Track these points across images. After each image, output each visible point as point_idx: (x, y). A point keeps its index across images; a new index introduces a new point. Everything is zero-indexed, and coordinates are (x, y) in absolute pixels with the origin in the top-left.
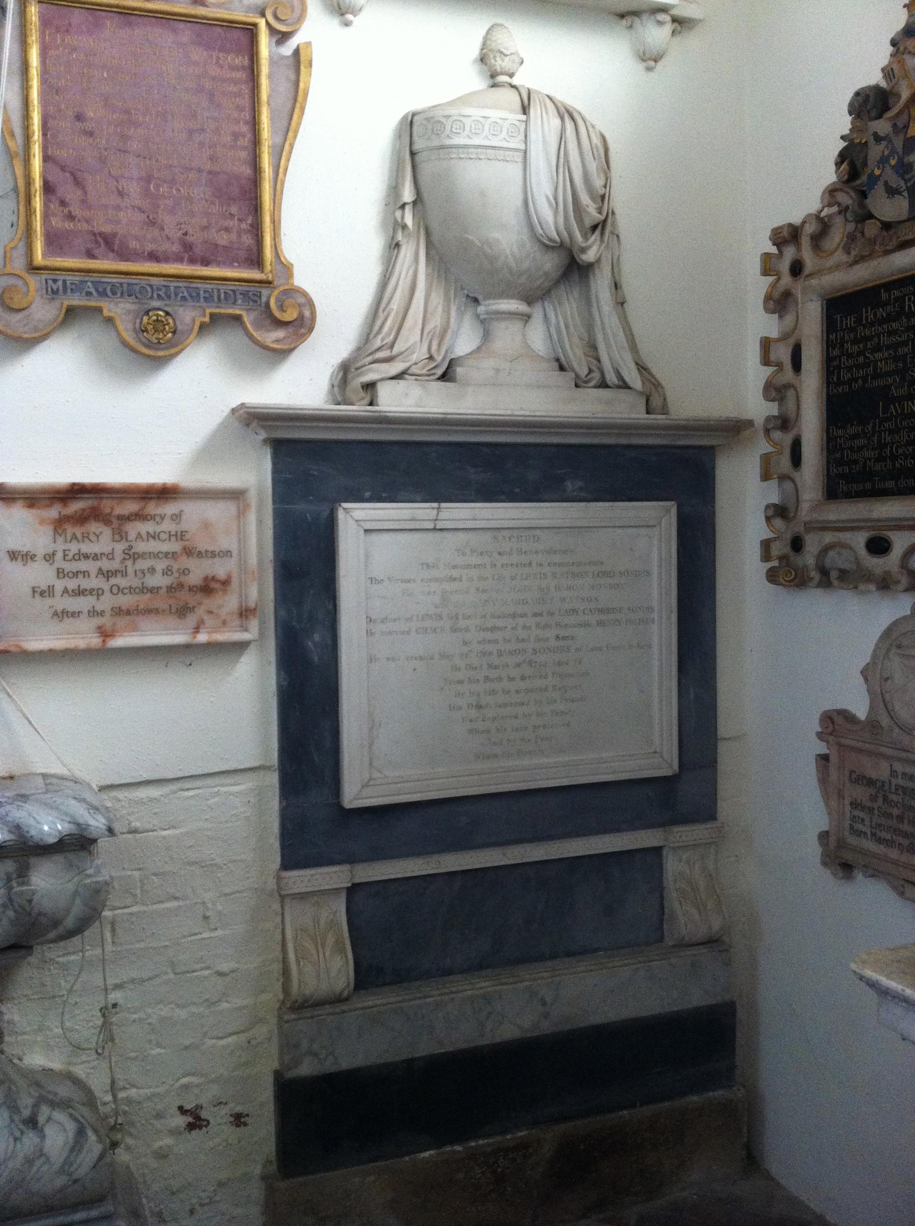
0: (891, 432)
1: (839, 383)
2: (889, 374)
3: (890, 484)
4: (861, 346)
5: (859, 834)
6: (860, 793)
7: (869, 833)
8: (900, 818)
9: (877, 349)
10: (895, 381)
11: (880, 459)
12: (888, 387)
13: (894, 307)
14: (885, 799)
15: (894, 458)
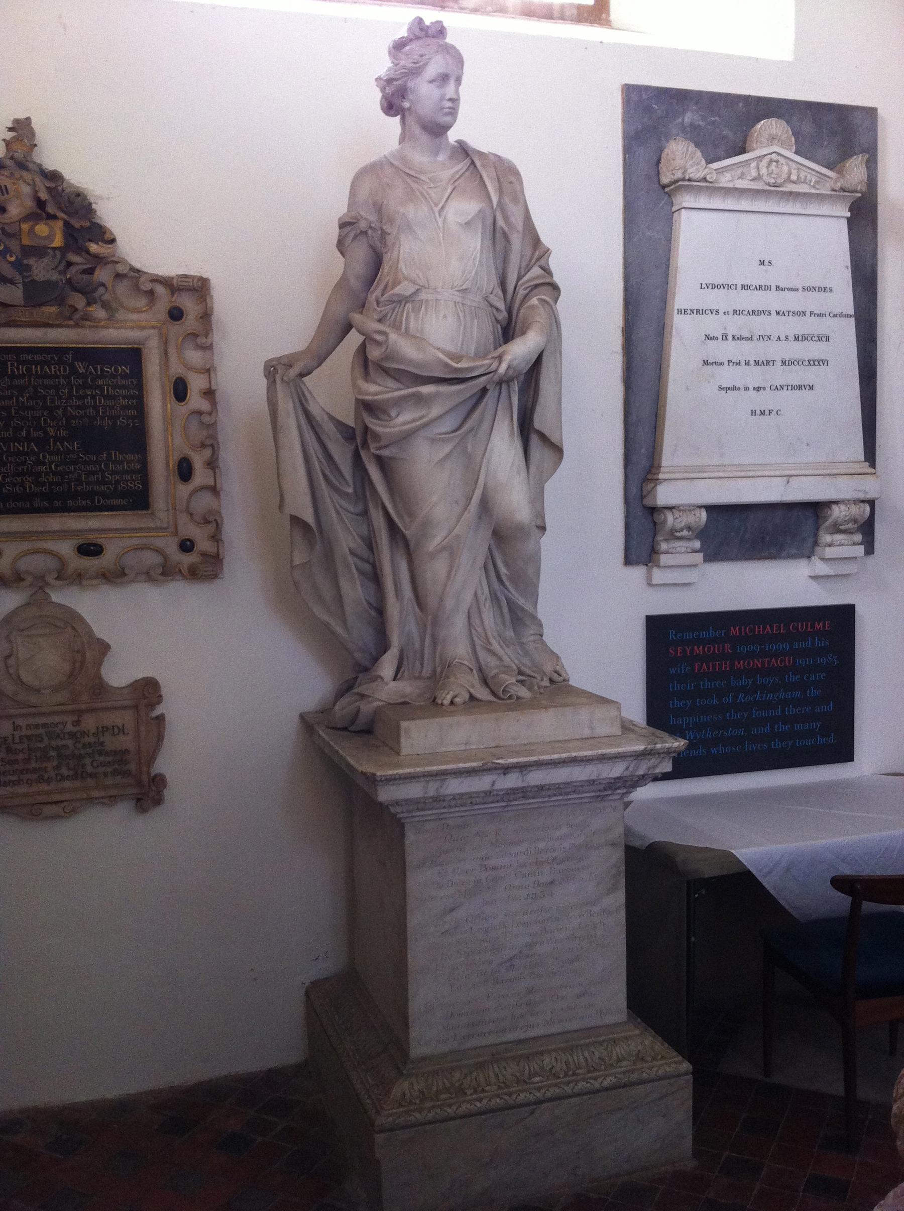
14: (9, 750)
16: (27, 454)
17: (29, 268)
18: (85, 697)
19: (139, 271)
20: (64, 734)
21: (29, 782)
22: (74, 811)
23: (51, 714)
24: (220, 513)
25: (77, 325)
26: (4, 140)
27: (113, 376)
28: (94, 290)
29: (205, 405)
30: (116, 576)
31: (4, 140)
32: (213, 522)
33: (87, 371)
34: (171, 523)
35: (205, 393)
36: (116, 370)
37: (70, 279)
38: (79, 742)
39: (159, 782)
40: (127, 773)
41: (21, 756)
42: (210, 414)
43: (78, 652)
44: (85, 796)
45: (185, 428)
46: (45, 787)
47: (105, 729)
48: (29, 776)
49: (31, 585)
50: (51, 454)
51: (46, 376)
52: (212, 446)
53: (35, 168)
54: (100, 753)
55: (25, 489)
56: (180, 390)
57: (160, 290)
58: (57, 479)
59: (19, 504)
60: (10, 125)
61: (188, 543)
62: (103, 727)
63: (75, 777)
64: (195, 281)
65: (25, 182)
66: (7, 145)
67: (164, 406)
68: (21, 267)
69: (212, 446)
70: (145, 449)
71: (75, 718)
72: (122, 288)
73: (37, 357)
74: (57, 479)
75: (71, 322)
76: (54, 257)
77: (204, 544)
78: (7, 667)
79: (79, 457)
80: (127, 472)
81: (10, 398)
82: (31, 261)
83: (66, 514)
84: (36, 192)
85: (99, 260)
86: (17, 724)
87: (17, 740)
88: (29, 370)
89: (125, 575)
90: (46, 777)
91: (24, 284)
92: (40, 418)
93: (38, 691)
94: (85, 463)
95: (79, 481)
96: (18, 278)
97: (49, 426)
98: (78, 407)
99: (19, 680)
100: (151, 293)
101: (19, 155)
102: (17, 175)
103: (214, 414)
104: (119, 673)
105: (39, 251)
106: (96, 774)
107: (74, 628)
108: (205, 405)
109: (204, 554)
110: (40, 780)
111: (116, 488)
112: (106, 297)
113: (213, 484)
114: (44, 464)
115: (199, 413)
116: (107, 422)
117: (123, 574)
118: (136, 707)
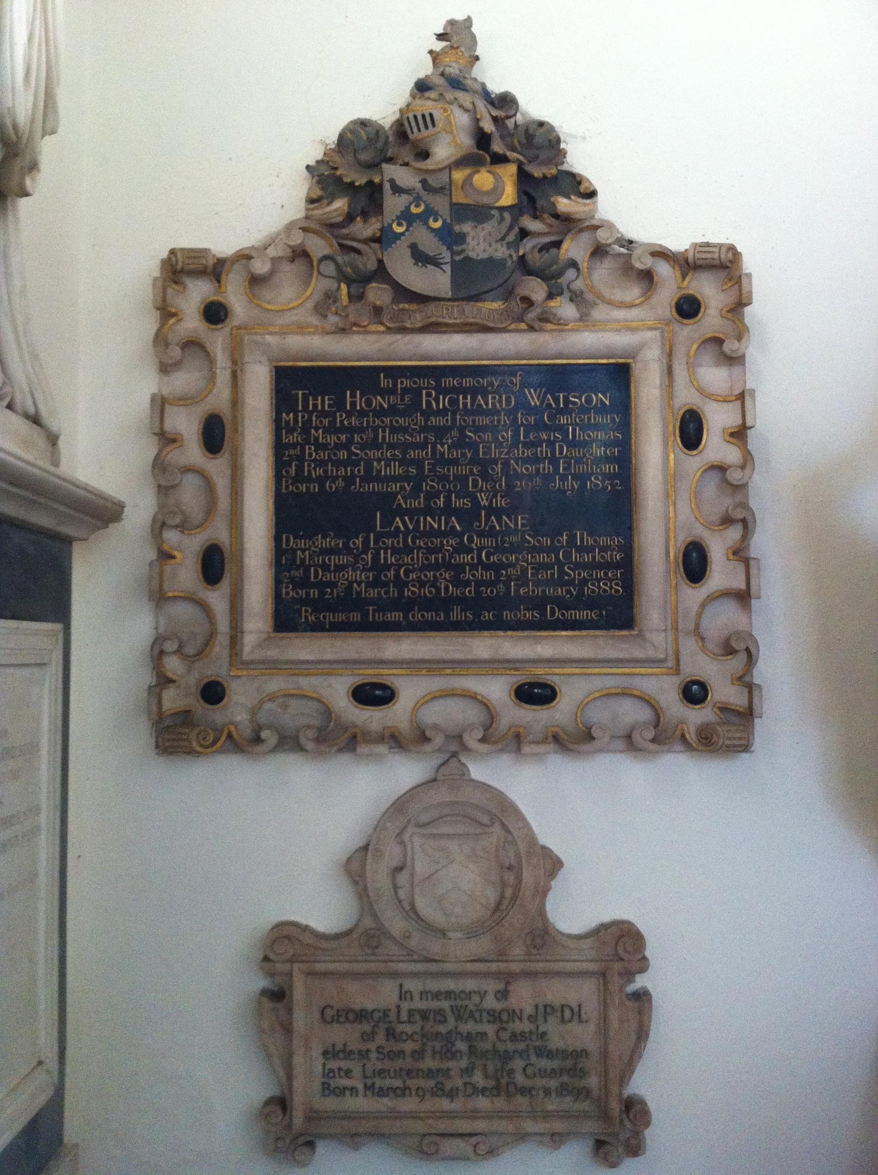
0: (395, 551)
1: (299, 478)
2: (395, 479)
3: (395, 616)
4: (343, 437)
5: (340, 1092)
6: (345, 1034)
7: (360, 1087)
8: (418, 1055)
9: (375, 445)
10: (402, 488)
11: (375, 583)
12: (394, 495)
13: (402, 399)
14: (391, 1034)
15: (400, 584)
16: (440, 534)
17: (461, 238)
18: (518, 951)
19: (631, 242)
20: (481, 1011)
21: (421, 1094)
22: (492, 1152)
23: (462, 975)
24: (751, 635)
25: (531, 328)
26: (431, 52)
27: (583, 410)
28: (560, 273)
29: (731, 454)
30: (576, 740)
31: (431, 52)
32: (740, 650)
33: (542, 403)
34: (670, 652)
35: (732, 435)
36: (589, 400)
37: (524, 255)
38: (505, 1029)
39: (635, 1111)
40: (582, 1093)
41: (409, 1046)
42: (743, 467)
43: (510, 868)
44: (511, 1128)
45: (697, 494)
46: (445, 1104)
47: (548, 1009)
48: (422, 1083)
49: (439, 750)
50: (481, 534)
51: (480, 411)
52: (744, 521)
53: (478, 87)
54: (541, 1052)
55: (438, 590)
56: (690, 429)
57: (663, 269)
58: (490, 575)
59: (429, 615)
60: (440, 31)
61: (695, 687)
62: (545, 1007)
63: (496, 1090)
64: (724, 250)
65: (461, 106)
66: (434, 60)
67: (666, 457)
68: (451, 238)
69: (744, 521)
70: (630, 528)
71: (501, 987)
72: (602, 275)
73: (468, 382)
74: (490, 575)
75: (523, 326)
76: (502, 219)
77: (724, 691)
78: (396, 888)
79: (524, 540)
80: (599, 566)
81: (423, 446)
82: (466, 227)
83: (501, 633)
84: (477, 121)
85: (568, 224)
86: (406, 987)
87: (404, 1016)
88: (454, 402)
89: (592, 738)
90: (448, 1086)
91: (454, 265)
92: (467, 477)
93: (443, 933)
94: (534, 550)
95: (522, 580)
96: (447, 256)
97: (481, 491)
98: (526, 461)
99: (412, 912)
100: (647, 277)
101: (453, 70)
102: (449, 96)
103: (748, 470)
104: (573, 911)
105: (478, 213)
106: (531, 1089)
107: (503, 825)
108: (731, 454)
109: (724, 709)
110: (439, 1091)
111: (581, 593)
112: (578, 285)
113: (743, 586)
114: (469, 551)
115: (721, 469)
116: (571, 484)
117: (588, 737)
118: (604, 974)
